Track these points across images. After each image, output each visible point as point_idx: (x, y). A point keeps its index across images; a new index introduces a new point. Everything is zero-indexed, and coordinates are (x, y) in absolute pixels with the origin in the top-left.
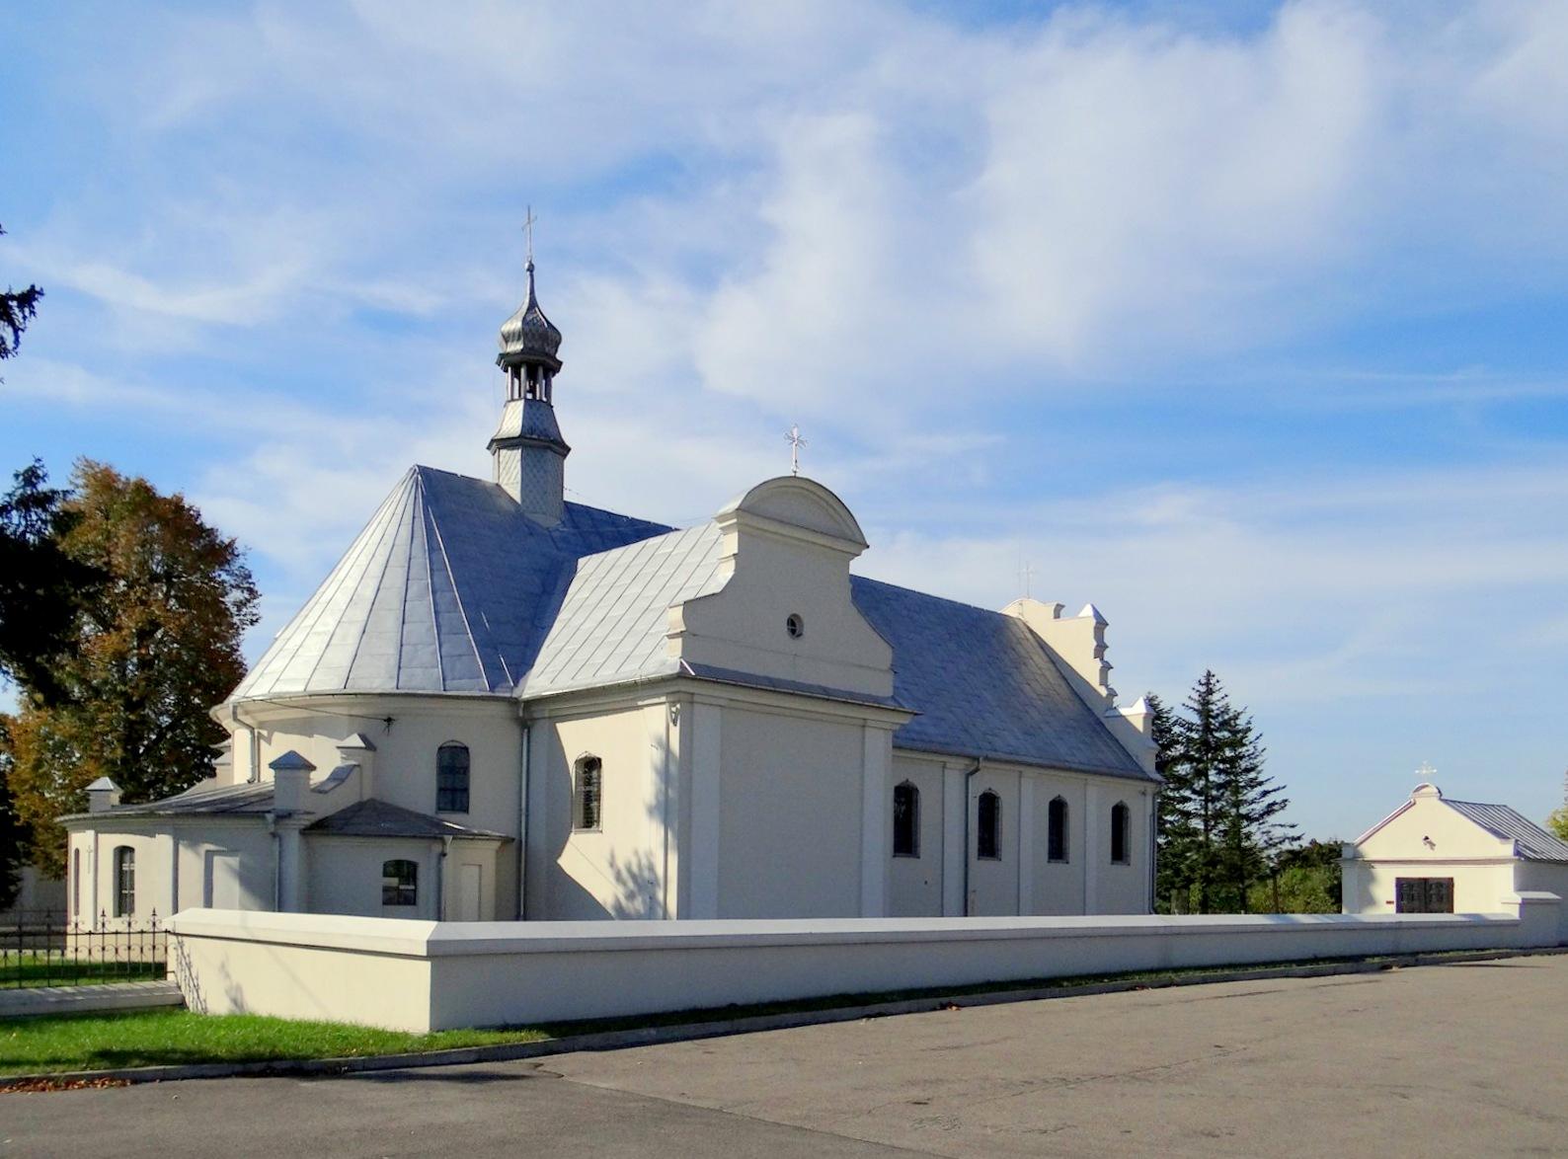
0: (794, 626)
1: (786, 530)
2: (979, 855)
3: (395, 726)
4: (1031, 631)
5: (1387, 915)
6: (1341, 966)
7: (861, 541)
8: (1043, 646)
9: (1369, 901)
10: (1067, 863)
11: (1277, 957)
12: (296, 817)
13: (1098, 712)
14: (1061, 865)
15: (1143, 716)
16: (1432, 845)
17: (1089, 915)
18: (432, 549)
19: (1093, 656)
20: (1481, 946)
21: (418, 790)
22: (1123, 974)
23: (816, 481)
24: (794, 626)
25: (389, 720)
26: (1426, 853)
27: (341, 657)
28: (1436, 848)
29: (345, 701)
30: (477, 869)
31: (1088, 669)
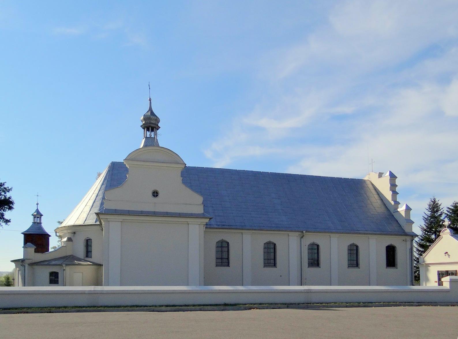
0: (155, 194)
1: (155, 164)
2: (387, 266)
3: (76, 235)
4: (372, 184)
5: (435, 286)
6: (215, 307)
7: (182, 162)
8: (376, 189)
9: (427, 280)
10: (320, 267)
11: (141, 304)
12: (25, 260)
13: (392, 210)
14: (395, 269)
15: (404, 210)
16: (449, 255)
17: (332, 285)
18: (103, 184)
19: (389, 190)
20: (328, 302)
21: (81, 252)
22: (9, 309)
23: (166, 148)
24: (155, 194)
25: (74, 233)
26: (446, 260)
27: (84, 216)
28: (450, 257)
29: (65, 229)
30: (81, 274)
31: (388, 195)
